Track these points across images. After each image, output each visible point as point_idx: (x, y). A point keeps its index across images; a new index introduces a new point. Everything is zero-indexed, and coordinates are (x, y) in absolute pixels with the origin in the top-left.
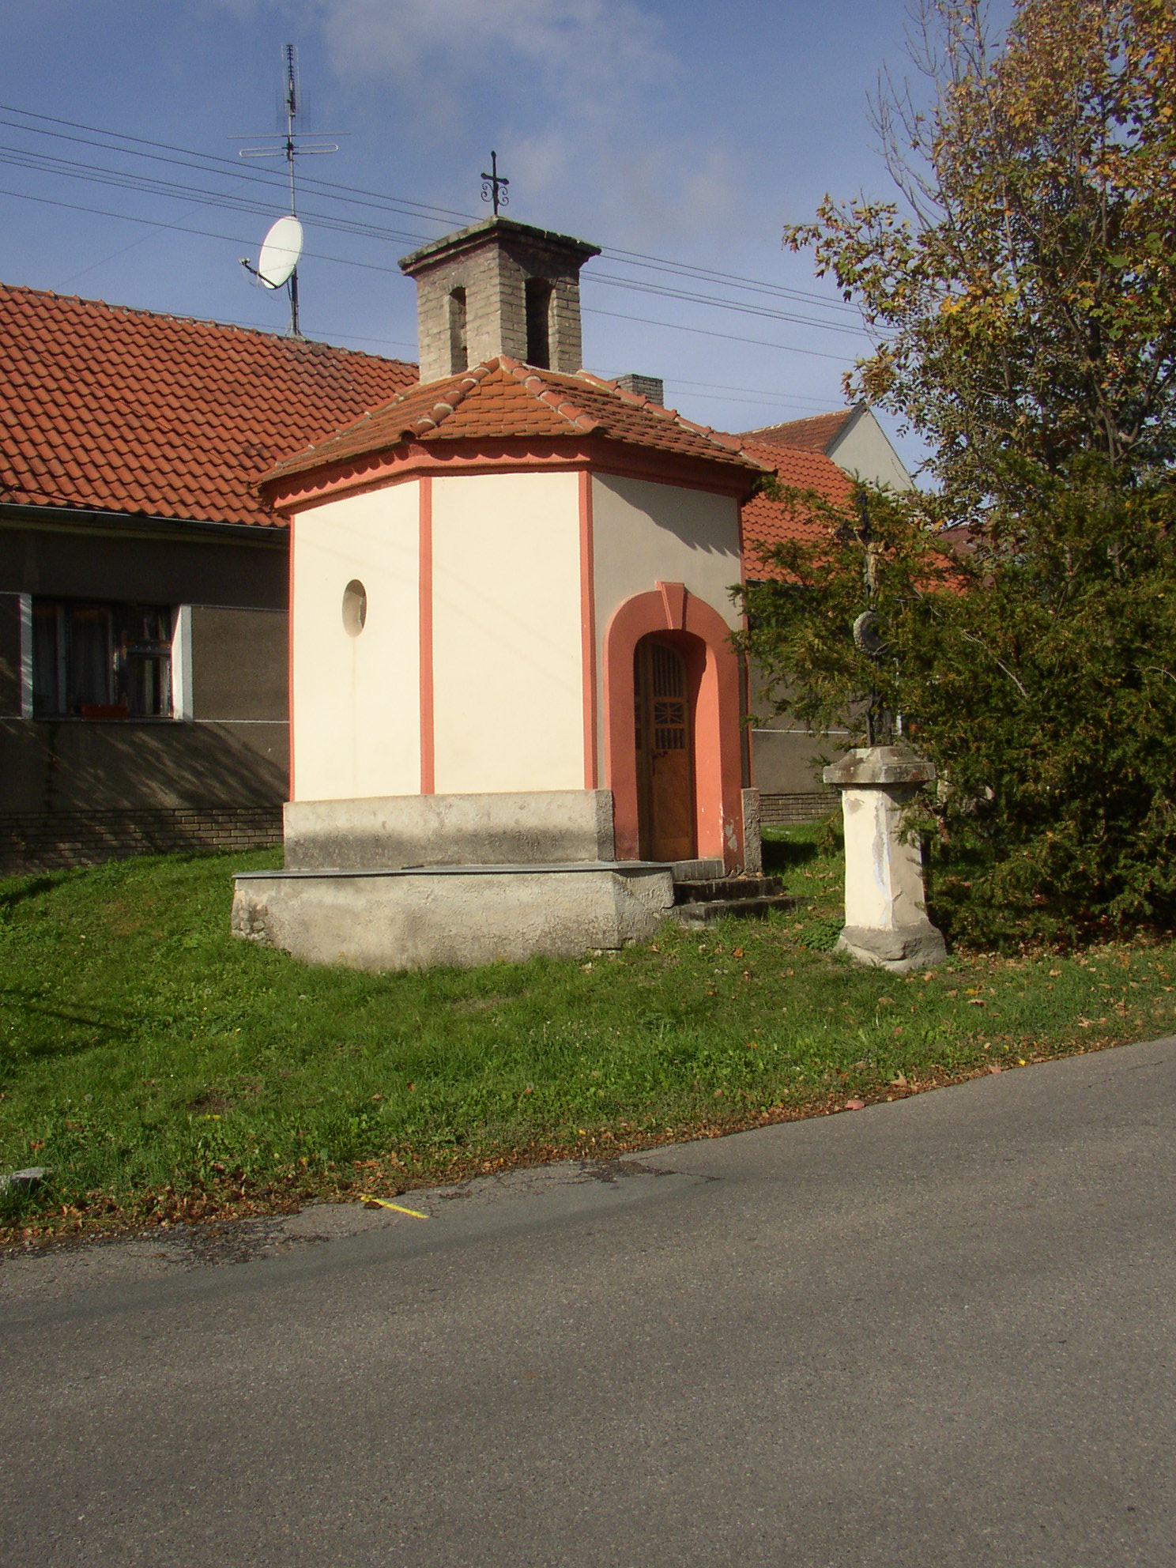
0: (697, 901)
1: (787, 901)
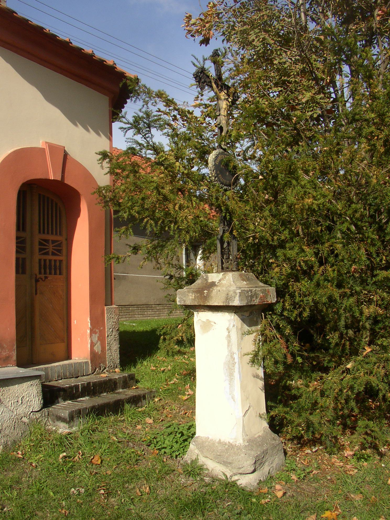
0: (65, 400)
1: (142, 393)
